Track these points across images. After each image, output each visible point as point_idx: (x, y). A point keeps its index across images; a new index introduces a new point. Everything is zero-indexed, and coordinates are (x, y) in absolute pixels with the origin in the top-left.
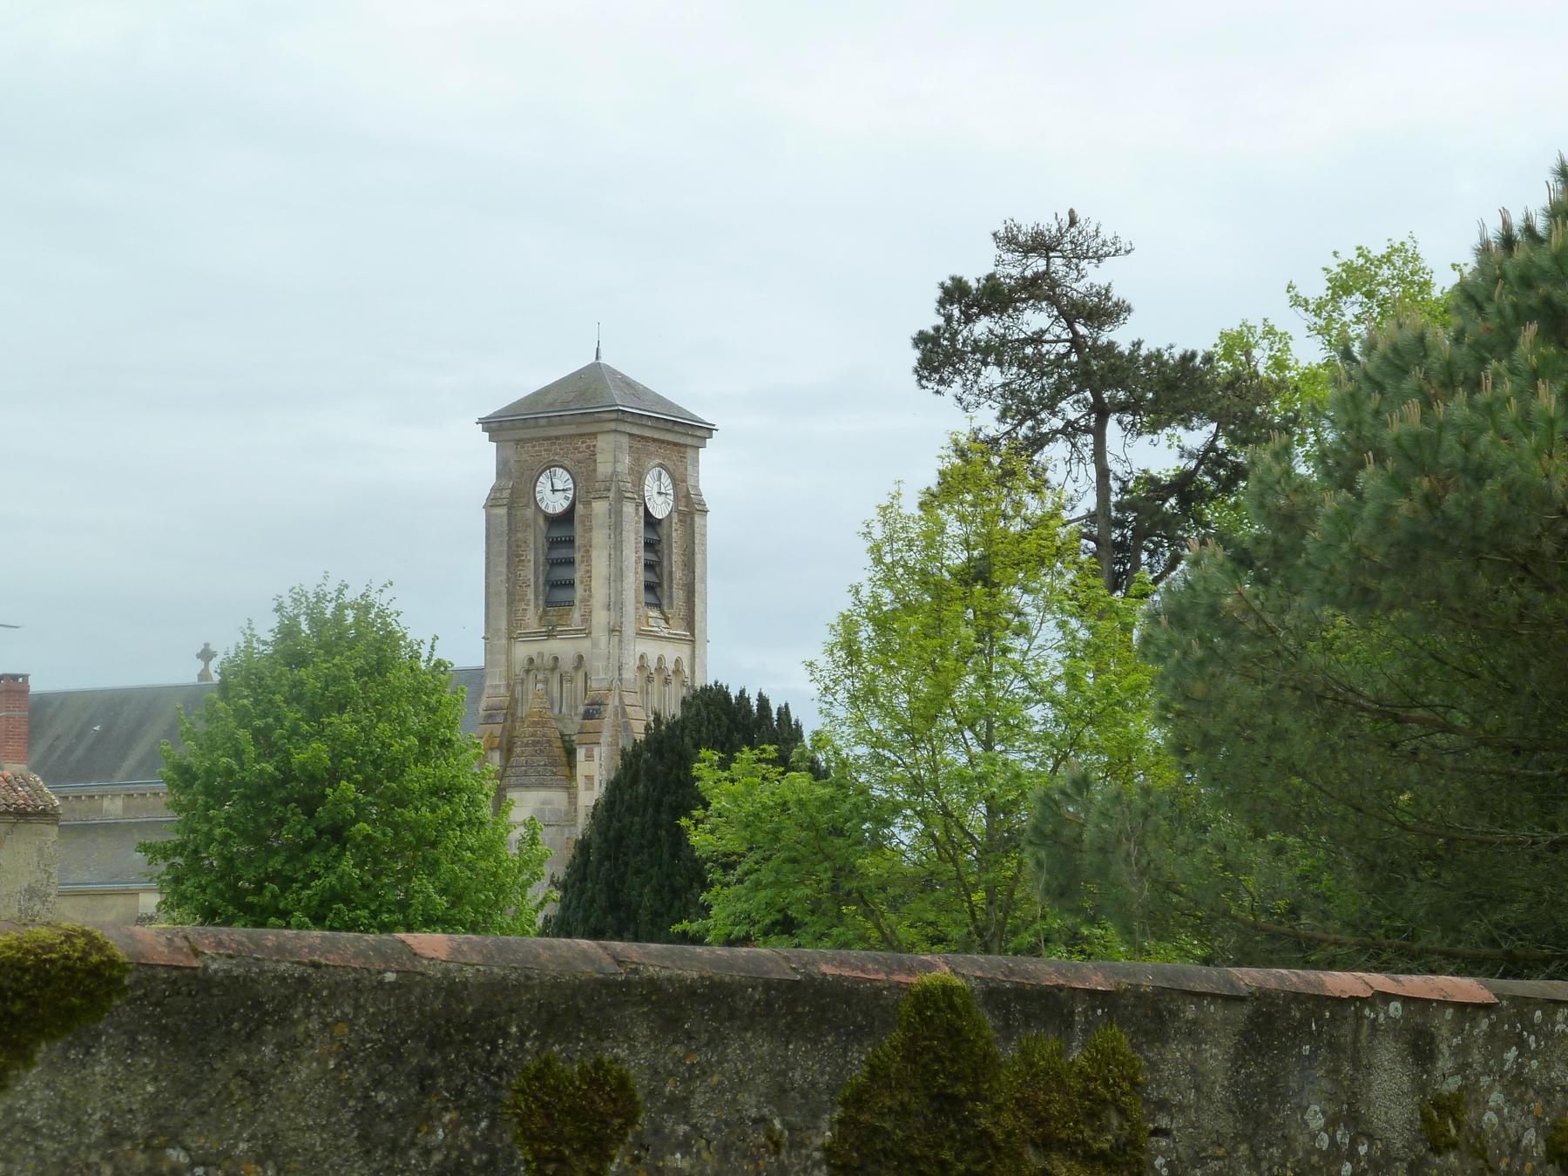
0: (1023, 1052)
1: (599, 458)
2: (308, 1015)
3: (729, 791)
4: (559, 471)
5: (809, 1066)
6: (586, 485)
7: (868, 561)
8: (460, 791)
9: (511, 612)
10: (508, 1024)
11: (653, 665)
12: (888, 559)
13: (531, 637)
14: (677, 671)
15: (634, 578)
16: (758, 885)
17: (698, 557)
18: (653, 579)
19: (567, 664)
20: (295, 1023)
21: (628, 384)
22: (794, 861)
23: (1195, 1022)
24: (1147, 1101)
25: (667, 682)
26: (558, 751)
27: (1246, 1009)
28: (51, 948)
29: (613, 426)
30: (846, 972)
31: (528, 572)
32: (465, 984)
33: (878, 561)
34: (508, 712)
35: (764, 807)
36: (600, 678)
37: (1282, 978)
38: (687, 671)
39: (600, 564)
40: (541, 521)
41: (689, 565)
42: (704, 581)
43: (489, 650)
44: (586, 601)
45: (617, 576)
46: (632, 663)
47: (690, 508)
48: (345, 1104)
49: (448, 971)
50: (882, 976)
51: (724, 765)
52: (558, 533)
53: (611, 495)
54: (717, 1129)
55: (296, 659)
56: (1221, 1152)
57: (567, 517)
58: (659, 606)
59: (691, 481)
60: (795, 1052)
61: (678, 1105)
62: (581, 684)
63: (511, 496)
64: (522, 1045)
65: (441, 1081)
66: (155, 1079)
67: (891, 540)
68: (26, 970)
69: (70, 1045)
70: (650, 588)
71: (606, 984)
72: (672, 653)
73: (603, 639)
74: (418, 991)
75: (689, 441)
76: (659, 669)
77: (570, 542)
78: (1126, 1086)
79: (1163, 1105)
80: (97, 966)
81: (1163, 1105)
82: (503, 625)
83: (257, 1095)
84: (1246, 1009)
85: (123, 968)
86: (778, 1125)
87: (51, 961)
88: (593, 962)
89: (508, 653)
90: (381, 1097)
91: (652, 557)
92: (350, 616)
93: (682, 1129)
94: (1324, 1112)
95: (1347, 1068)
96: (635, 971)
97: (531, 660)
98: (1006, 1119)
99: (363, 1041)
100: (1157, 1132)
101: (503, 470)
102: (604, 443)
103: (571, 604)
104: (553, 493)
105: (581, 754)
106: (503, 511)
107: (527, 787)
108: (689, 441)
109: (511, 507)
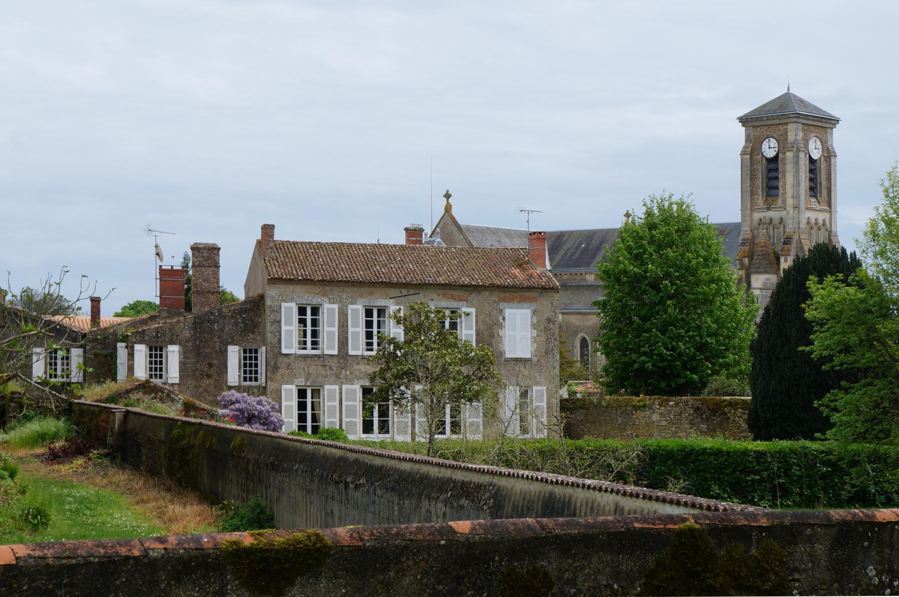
0: (728, 552)
1: (789, 134)
2: (408, 559)
3: (823, 293)
4: (772, 139)
5: (628, 564)
6: (782, 141)
7: (882, 195)
8: (721, 281)
9: (752, 199)
10: (495, 556)
11: (813, 222)
12: (891, 195)
13: (759, 210)
14: (824, 224)
15: (804, 185)
16: (834, 334)
17: (833, 176)
18: (813, 185)
19: (776, 221)
20: (403, 563)
21: (801, 101)
22: (850, 324)
23: (810, 536)
24: (788, 568)
25: (819, 229)
26: (772, 258)
27: (836, 529)
28: (301, 542)
29: (795, 120)
30: (646, 526)
31: (759, 182)
32: (475, 543)
33: (887, 196)
34: (751, 242)
35: (836, 301)
36: (790, 227)
37: (855, 514)
38: (828, 225)
39: (789, 179)
40: (764, 161)
41: (829, 179)
42: (835, 186)
43: (743, 216)
44: (784, 194)
45: (797, 184)
46: (804, 221)
47: (829, 154)
48: (425, 591)
49: (468, 538)
50: (662, 526)
51: (820, 282)
52: (772, 166)
53: (794, 149)
54: (588, 590)
55: (652, 226)
56: (825, 587)
57: (775, 159)
58: (816, 197)
59: (829, 143)
60: (622, 559)
61: (572, 582)
62: (782, 230)
63: (752, 150)
64: (501, 564)
65: (466, 580)
66: (345, 587)
67: (893, 186)
68: (289, 552)
69: (310, 577)
70: (811, 189)
71: (538, 538)
72: (821, 217)
73: (791, 211)
74: (455, 547)
75: (829, 125)
76: (816, 224)
77: (777, 170)
78: (777, 563)
79: (796, 570)
80: (319, 548)
81: (796, 570)
82: (749, 205)
83: (388, 590)
84: (836, 529)
85: (330, 548)
86: (616, 586)
87: (300, 548)
88: (532, 529)
89: (751, 217)
90: (441, 588)
91: (813, 176)
92: (675, 207)
93: (573, 591)
94: (875, 569)
95: (887, 551)
96: (550, 532)
97: (761, 220)
98: (721, 579)
99: (432, 567)
100: (794, 580)
101: (748, 139)
102: (791, 127)
103: (778, 196)
104: (769, 149)
105: (782, 259)
106: (748, 157)
107: (760, 273)
108: (829, 125)
109: (751, 154)
